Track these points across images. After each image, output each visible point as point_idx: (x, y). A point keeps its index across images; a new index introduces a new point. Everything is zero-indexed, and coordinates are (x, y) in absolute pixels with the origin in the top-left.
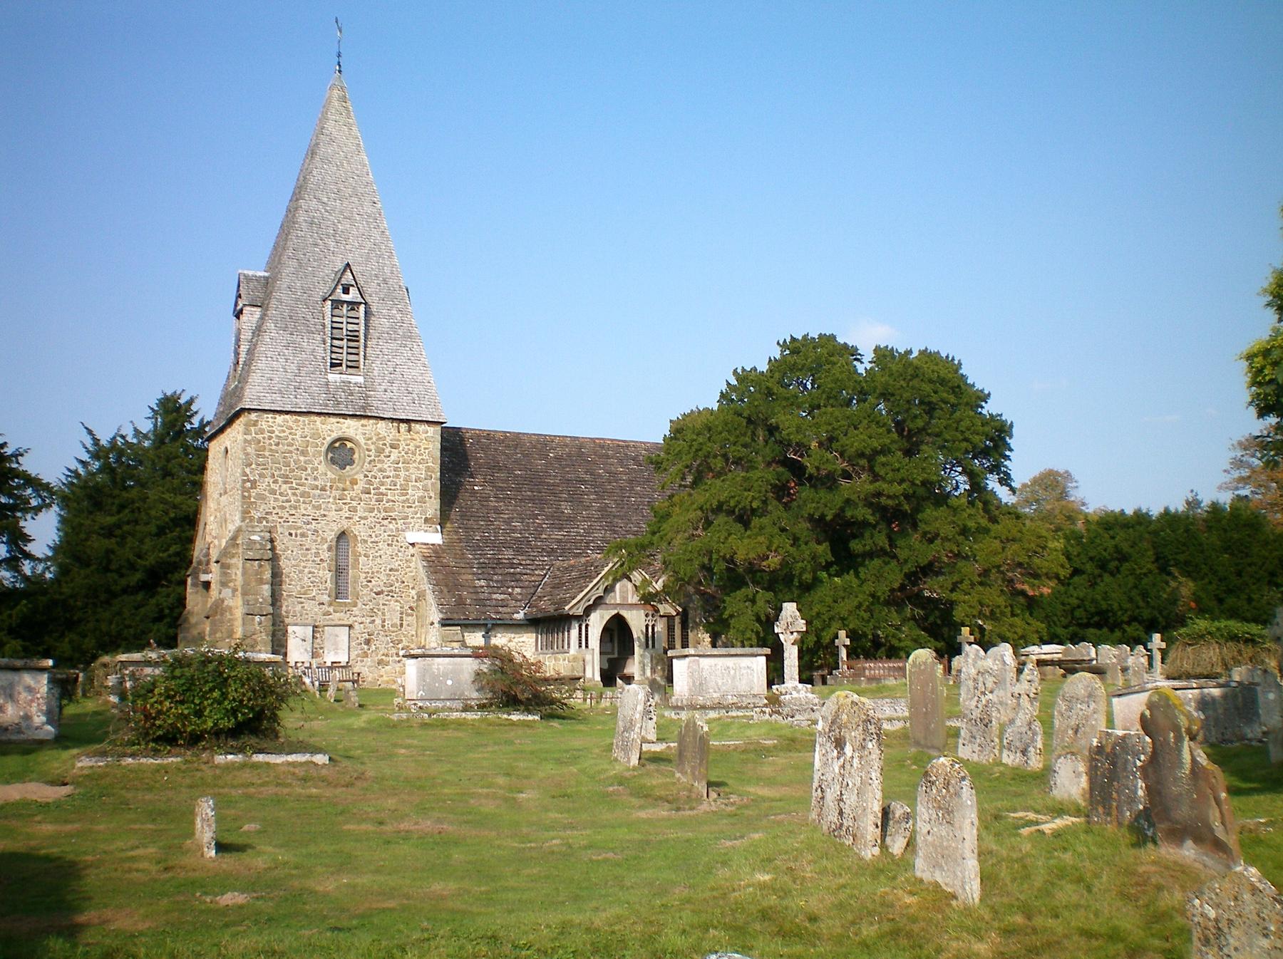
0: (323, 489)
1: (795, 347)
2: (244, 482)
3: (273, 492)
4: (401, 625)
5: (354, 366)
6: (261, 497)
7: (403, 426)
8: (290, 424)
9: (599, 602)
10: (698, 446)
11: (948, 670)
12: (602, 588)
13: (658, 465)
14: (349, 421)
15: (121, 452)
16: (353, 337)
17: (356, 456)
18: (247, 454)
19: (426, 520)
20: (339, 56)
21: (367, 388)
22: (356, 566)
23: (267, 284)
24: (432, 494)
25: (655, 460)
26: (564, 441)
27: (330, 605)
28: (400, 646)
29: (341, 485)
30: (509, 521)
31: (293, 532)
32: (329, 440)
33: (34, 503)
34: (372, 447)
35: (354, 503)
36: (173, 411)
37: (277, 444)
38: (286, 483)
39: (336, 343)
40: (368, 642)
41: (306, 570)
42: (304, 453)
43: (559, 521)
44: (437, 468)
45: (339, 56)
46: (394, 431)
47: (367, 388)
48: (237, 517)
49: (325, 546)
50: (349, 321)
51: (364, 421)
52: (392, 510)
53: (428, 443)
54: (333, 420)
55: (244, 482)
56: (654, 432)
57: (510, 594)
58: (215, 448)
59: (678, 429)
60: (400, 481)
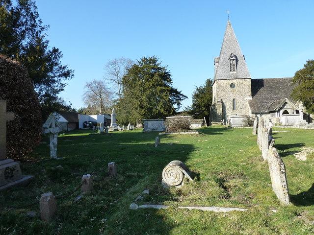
9: (281, 108)
10: (299, 75)
11: (178, 225)
13: (293, 81)
23: (219, 58)
25: (293, 81)
26: (276, 79)
33: (182, 99)
43: (275, 94)
44: (250, 87)
50: (235, 61)
53: (249, 82)
56: (292, 75)
58: (213, 86)
59: (297, 74)
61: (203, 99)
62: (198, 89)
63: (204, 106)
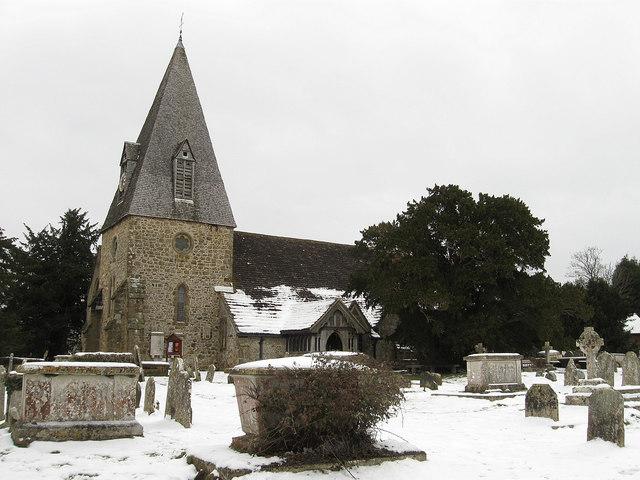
3: (144, 261)
6: (138, 264)
7: (214, 228)
20: (572, 427)
40: (193, 345)
42: (161, 240)
45: (572, 427)
48: (124, 274)
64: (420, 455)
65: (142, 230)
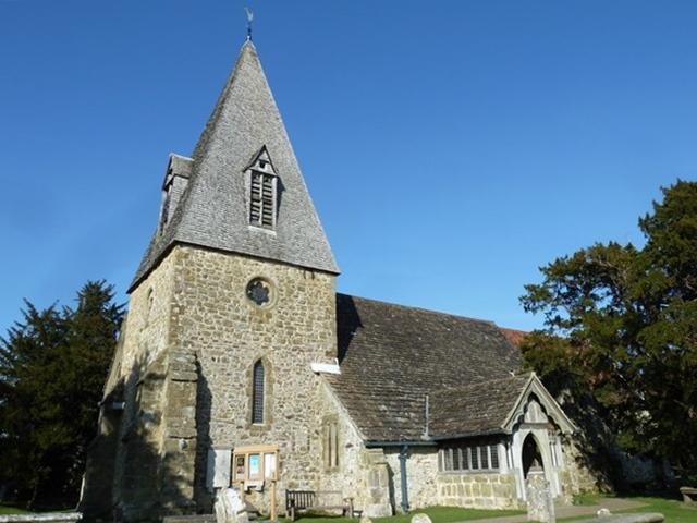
0: (243, 320)
1: (670, 195)
2: (173, 307)
3: (199, 319)
4: (309, 448)
5: (267, 223)
6: (186, 322)
7: (308, 273)
8: (217, 260)
12: (521, 409)
14: (266, 264)
15: (53, 323)
16: (267, 202)
17: (270, 295)
18: (177, 282)
19: (327, 353)
21: (281, 239)
22: (270, 393)
24: (331, 332)
26: (398, 309)
27: (247, 429)
28: (308, 468)
29: (258, 318)
30: (381, 359)
31: (216, 357)
32: (249, 278)
34: (284, 288)
35: (270, 335)
36: (95, 296)
37: (205, 276)
38: (210, 311)
39: (255, 203)
41: (227, 394)
42: (228, 287)
44: (334, 310)
46: (301, 277)
47: (281, 239)
49: (244, 372)
51: (278, 266)
52: (299, 342)
54: (252, 261)
55: (173, 307)
57: (409, 418)
60: (306, 319)
61: (53, 366)
62: (34, 318)
63: (54, 400)
64: (25, 299)
65: (196, 267)
